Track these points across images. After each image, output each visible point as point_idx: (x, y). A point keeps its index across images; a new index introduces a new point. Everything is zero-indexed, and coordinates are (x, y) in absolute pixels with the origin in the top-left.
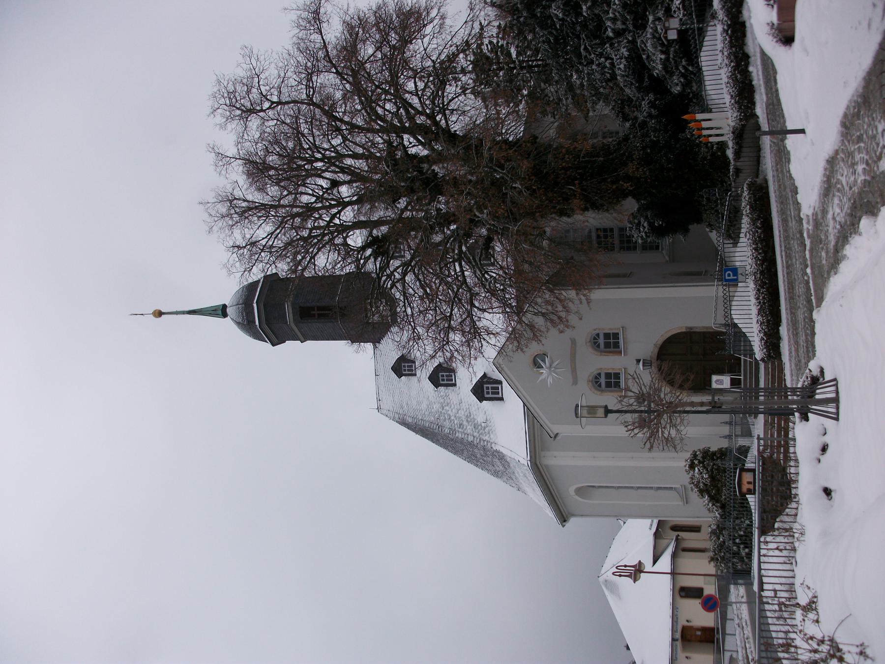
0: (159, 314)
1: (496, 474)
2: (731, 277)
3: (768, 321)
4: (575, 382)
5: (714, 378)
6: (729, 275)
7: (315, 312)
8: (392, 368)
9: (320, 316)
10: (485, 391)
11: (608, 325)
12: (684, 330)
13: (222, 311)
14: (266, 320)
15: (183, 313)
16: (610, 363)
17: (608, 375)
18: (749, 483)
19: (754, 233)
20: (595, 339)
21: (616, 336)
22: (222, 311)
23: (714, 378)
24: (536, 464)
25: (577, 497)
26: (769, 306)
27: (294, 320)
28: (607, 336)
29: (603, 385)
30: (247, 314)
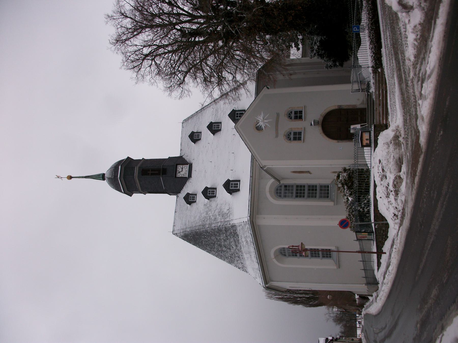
0: (70, 178)
1: (231, 262)
2: (357, 30)
3: (375, 47)
4: (277, 136)
5: (352, 127)
6: (355, 29)
8: (184, 198)
9: (152, 174)
10: (231, 186)
11: (296, 106)
12: (337, 108)
13: (102, 177)
14: (124, 175)
15: (83, 177)
16: (296, 125)
17: (295, 134)
18: (367, 140)
19: (368, 7)
20: (289, 114)
21: (300, 133)
22: (102, 177)
24: (253, 221)
25: (275, 260)
26: (375, 39)
27: (138, 176)
28: (296, 113)
29: (292, 138)
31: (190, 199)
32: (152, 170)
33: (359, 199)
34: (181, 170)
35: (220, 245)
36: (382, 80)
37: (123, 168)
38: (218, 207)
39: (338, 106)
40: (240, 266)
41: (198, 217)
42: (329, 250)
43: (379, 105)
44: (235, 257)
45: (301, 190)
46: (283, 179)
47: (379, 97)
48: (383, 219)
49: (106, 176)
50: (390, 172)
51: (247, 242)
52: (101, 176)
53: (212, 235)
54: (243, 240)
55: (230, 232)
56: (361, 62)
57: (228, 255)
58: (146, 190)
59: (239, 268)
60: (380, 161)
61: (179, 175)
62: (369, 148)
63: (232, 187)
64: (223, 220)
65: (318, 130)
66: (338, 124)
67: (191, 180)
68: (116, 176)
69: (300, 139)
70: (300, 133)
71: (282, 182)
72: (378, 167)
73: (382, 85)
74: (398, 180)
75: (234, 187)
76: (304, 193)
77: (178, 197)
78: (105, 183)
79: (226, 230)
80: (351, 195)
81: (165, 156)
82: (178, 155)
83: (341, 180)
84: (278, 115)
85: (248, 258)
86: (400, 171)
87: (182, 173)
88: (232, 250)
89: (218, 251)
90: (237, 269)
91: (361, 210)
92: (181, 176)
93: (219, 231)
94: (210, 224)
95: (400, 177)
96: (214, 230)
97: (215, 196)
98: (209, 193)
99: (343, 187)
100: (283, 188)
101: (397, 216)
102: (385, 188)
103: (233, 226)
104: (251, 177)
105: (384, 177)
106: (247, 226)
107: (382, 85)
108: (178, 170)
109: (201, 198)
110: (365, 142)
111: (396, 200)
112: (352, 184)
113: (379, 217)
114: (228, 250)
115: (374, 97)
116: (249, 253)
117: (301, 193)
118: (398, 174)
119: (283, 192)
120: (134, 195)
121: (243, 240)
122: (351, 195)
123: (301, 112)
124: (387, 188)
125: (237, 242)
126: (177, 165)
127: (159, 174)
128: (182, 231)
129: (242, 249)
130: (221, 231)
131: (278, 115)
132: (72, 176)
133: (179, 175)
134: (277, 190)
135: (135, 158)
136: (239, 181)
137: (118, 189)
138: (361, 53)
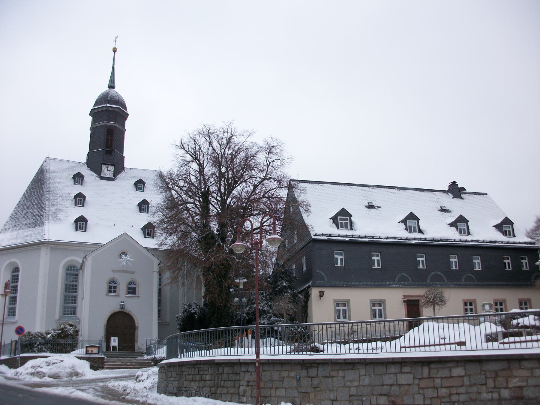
0: (115, 50)
4: (113, 271)
5: (116, 338)
7: (110, 138)
9: (107, 139)
11: (141, 290)
12: (136, 325)
13: (112, 86)
14: (109, 110)
15: (113, 64)
16: (122, 289)
18: (92, 351)
21: (115, 292)
22: (112, 86)
23: (116, 338)
24: (44, 244)
25: (8, 262)
29: (111, 285)
30: (113, 101)
31: (78, 178)
32: (111, 140)
33: (47, 344)
34: (109, 169)
35: (28, 208)
36: (143, 365)
37: (116, 110)
38: (65, 208)
39: (138, 327)
40: (7, 227)
41: (58, 186)
42: (14, 315)
43: (122, 362)
44: (16, 222)
45: (73, 289)
46: (83, 272)
47: (129, 363)
48: (23, 364)
49: (112, 90)
50: (50, 369)
51: (27, 236)
52: (112, 85)
53: (39, 200)
54: (30, 233)
55: (38, 221)
56: (462, 330)
57: (19, 215)
58: (94, 130)
59: (5, 226)
60: (62, 361)
61: (104, 168)
62: (85, 353)
63: (81, 223)
64: (51, 213)
65: (117, 309)
66: (121, 326)
67: (98, 179)
68: (109, 102)
69: (110, 291)
70: (115, 292)
71: (81, 271)
72: (58, 360)
73: (139, 365)
74: (42, 375)
75: (80, 226)
76: (69, 292)
77: (84, 164)
78: (105, 89)
79: (41, 216)
80: (53, 336)
81: (126, 153)
82: (126, 166)
83: (66, 328)
84: (133, 273)
85: (13, 235)
86: (49, 377)
87: (106, 170)
88: (22, 220)
89: (24, 205)
90: (4, 223)
91: (36, 345)
92: (103, 169)
93: (41, 209)
94: (49, 200)
95: (44, 376)
96: (43, 203)
97: (76, 205)
98: (80, 199)
99: (60, 330)
100: (75, 272)
101: (16, 375)
102: (39, 364)
103: (43, 223)
104: (86, 244)
105: (48, 364)
106: (40, 238)
107: (139, 365)
108: (109, 166)
109: (77, 189)
110: (90, 350)
111: (27, 373)
112: (63, 338)
113: (24, 360)
114: (23, 216)
115: (139, 358)
116: (17, 238)
117: (69, 289)
118: (47, 375)
119: (72, 272)
120: (90, 118)
121: (30, 233)
122: (53, 336)
123: (134, 293)
124: (39, 367)
125: (28, 226)
126: (114, 165)
127: (107, 146)
128: (47, 168)
129: (22, 231)
130: (41, 210)
131: (133, 273)
132: (116, 53)
133: (104, 168)
134: (74, 267)
135: (127, 122)
136: (85, 231)
137: (97, 103)
138: (462, 330)
